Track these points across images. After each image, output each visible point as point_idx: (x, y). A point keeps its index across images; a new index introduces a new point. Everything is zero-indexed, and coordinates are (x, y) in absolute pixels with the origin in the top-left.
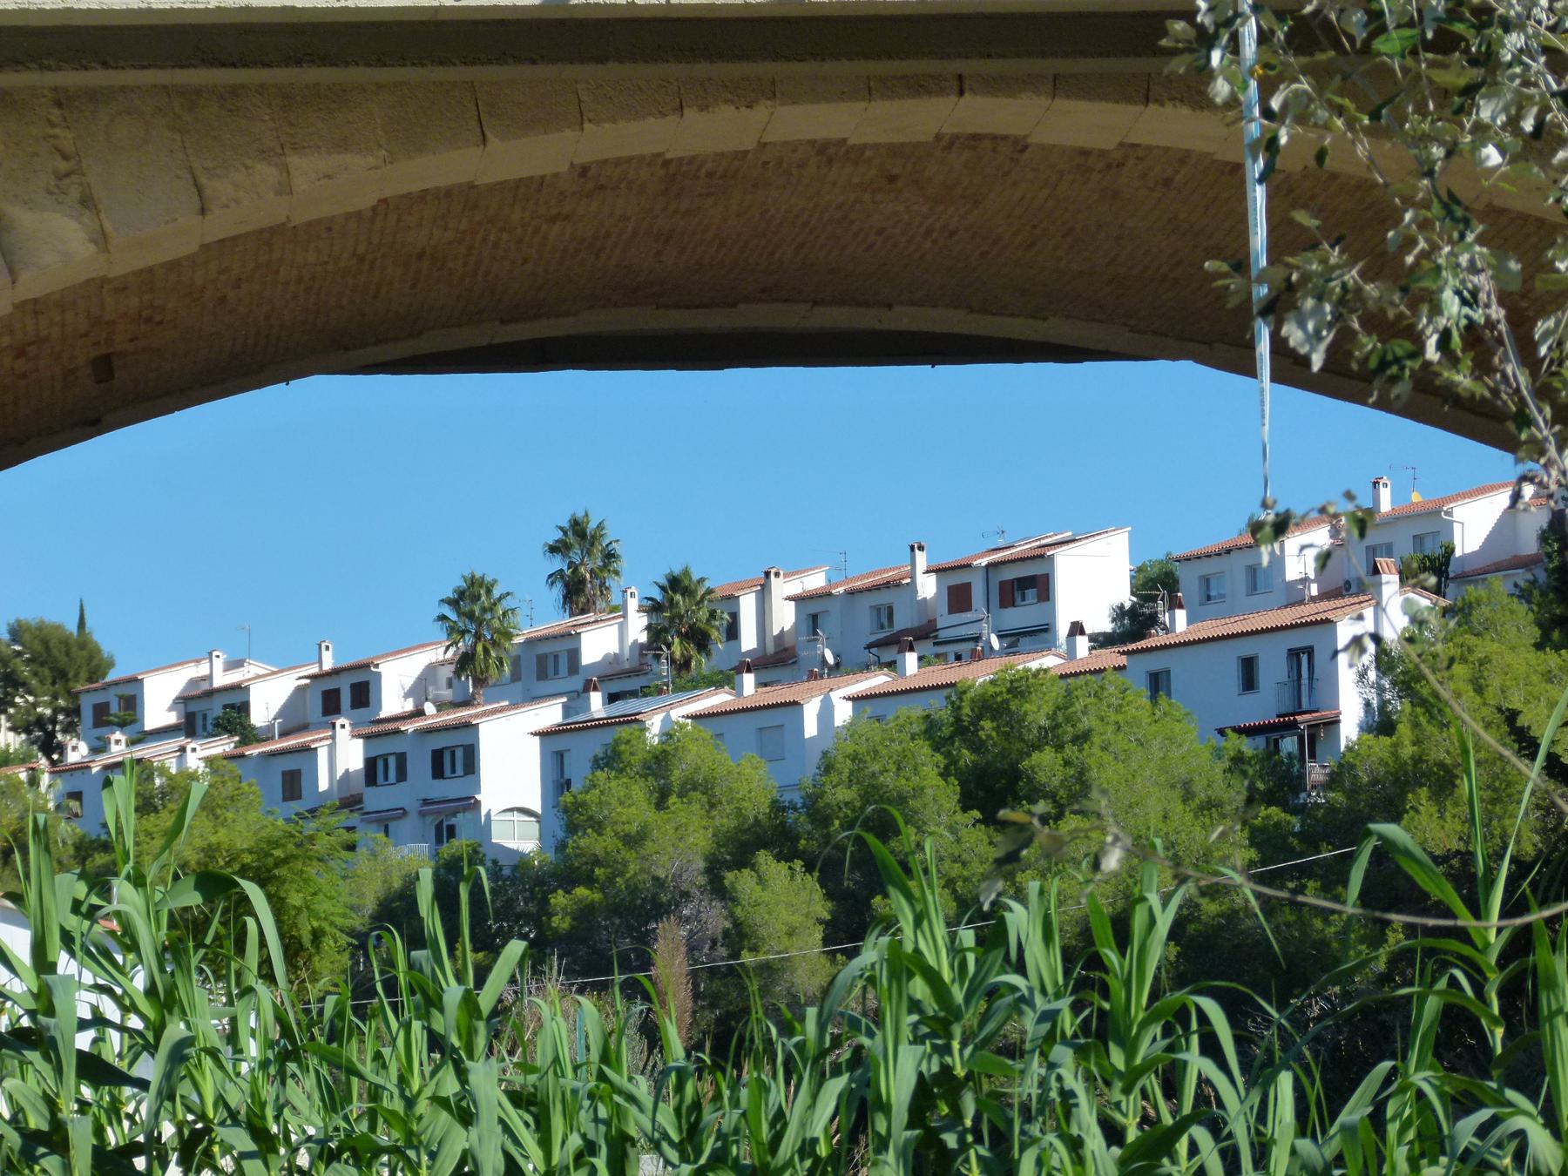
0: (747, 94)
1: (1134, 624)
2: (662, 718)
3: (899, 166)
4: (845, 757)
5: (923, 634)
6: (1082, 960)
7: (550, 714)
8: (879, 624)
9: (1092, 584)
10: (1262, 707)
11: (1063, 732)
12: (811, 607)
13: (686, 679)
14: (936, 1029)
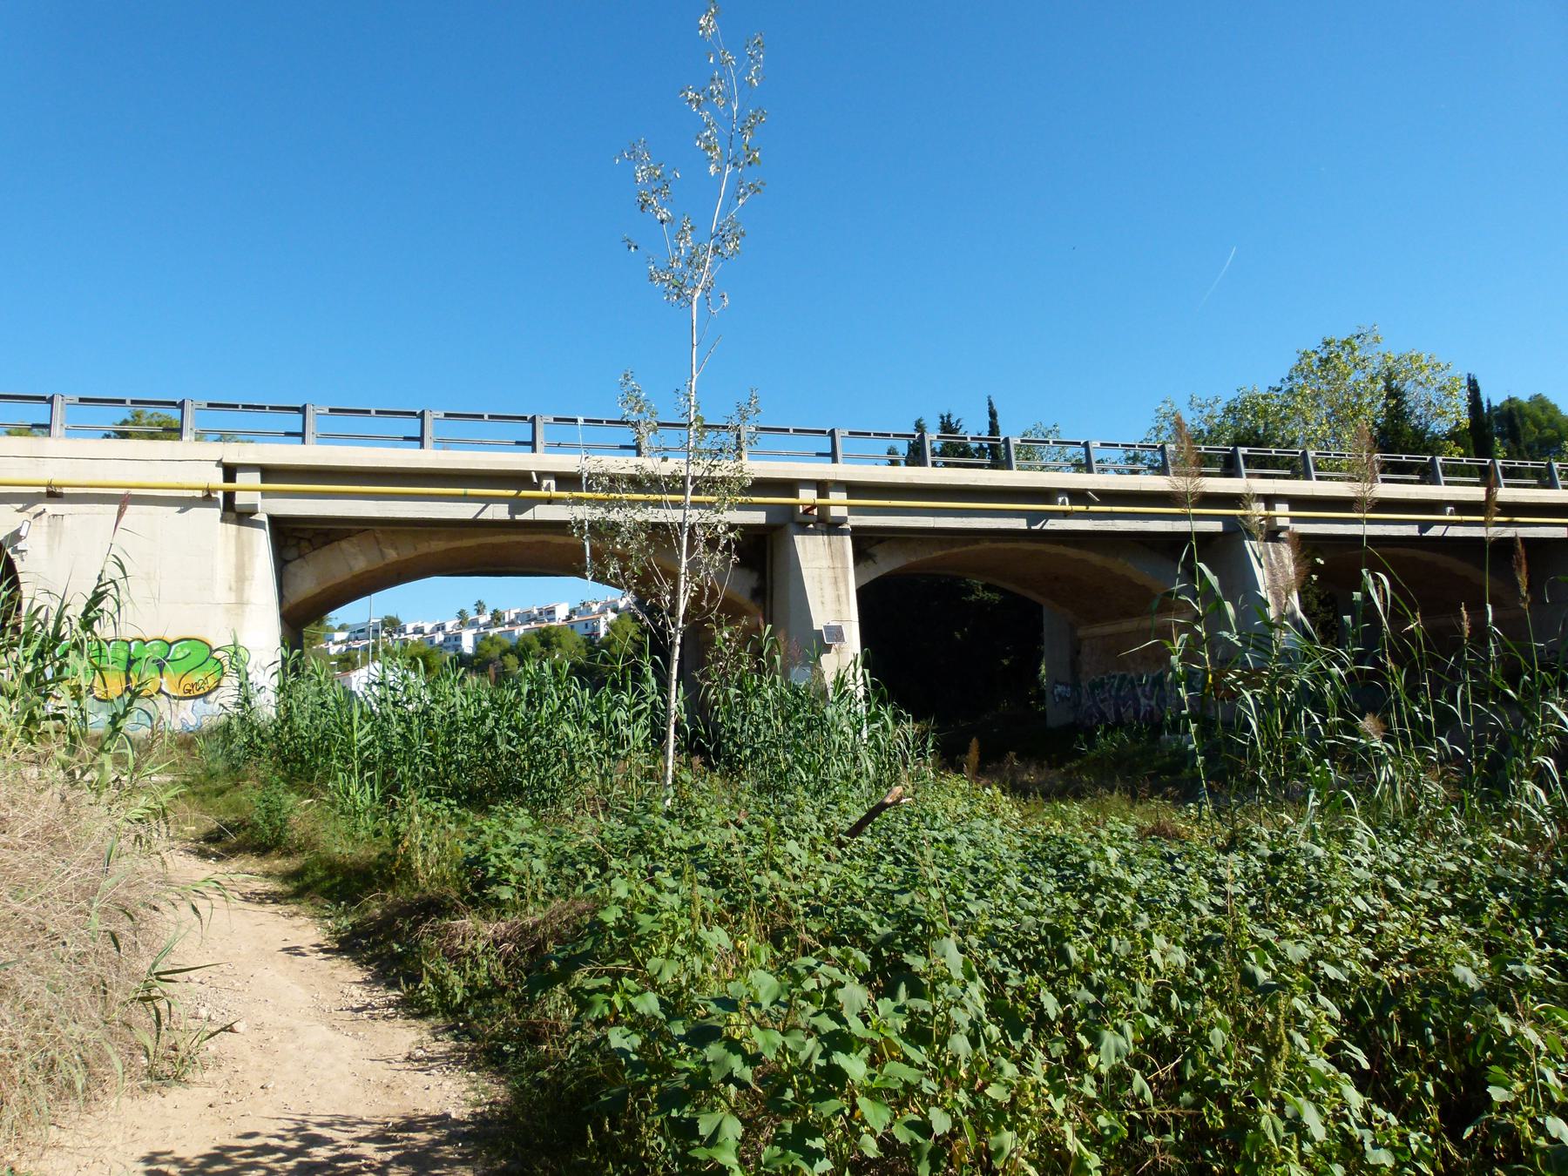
0: (506, 533)
1: (569, 618)
2: (492, 632)
3: (529, 546)
4: (522, 639)
5: (535, 619)
6: (555, 673)
7: (475, 631)
8: (528, 618)
9: (562, 612)
10: (588, 631)
11: (557, 635)
12: (517, 615)
13: (496, 625)
14: (531, 682)
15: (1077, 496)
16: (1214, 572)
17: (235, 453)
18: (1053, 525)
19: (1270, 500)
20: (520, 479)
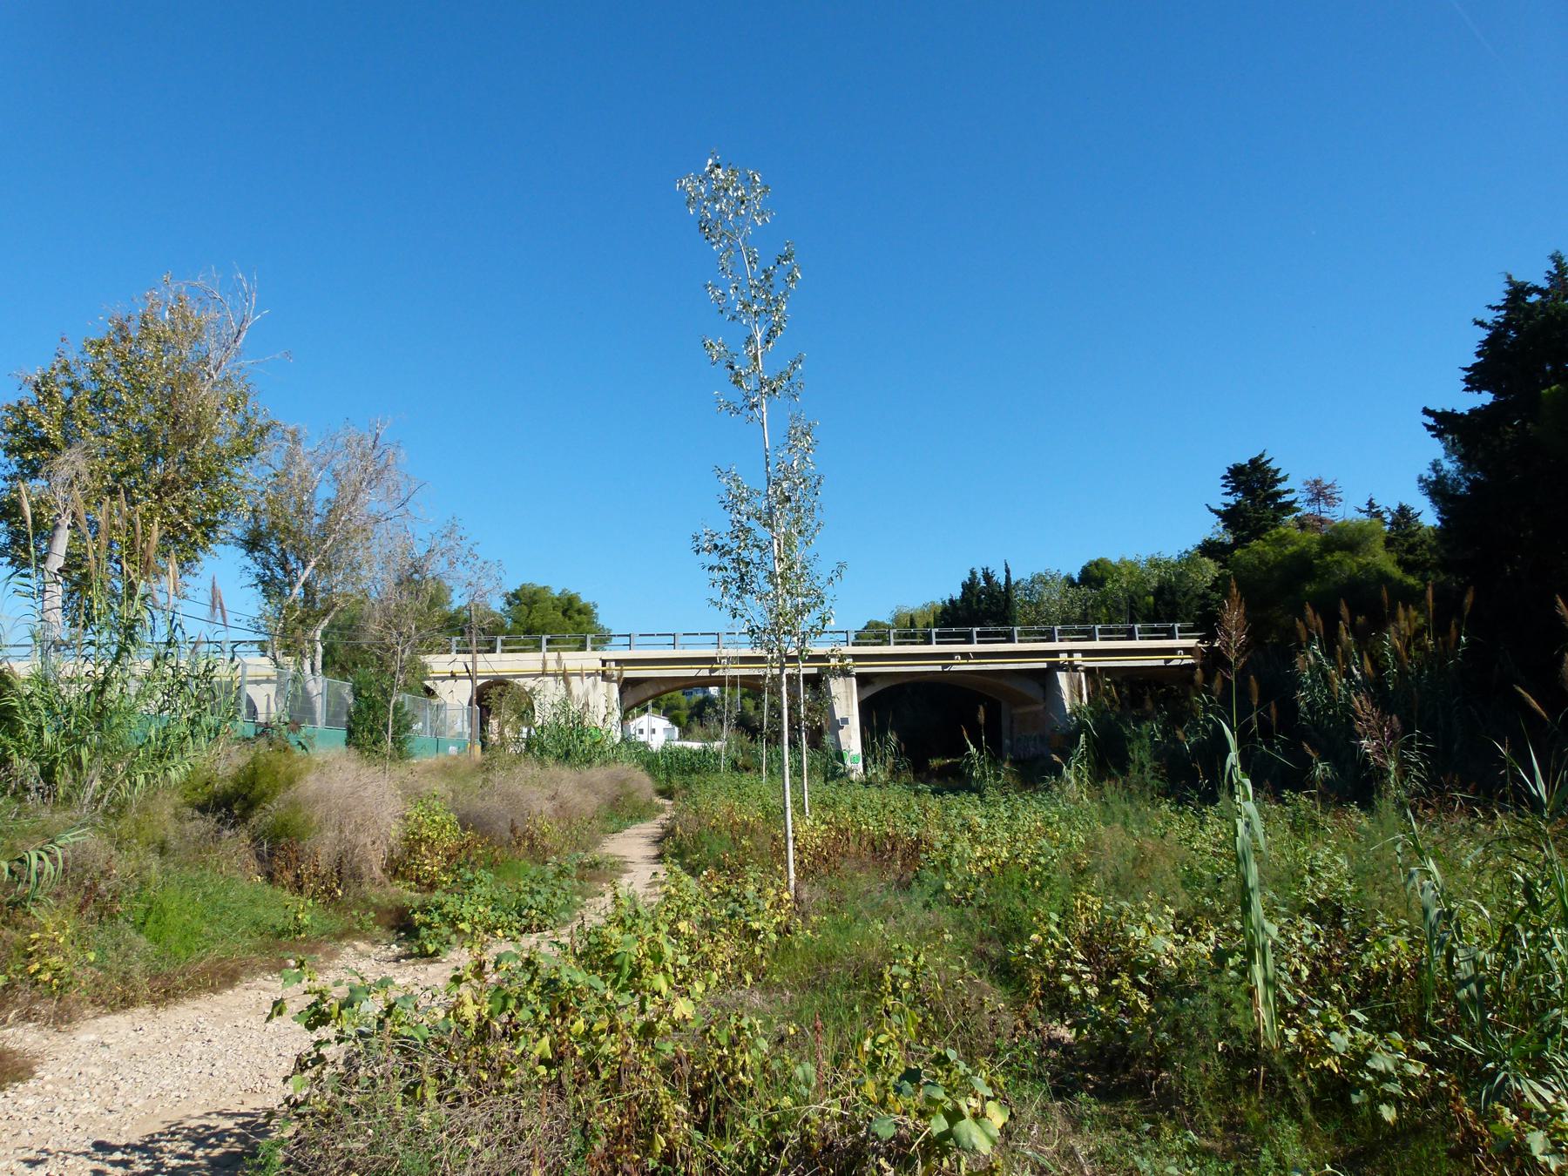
15: (965, 655)
16: (1534, 711)
17: (606, 655)
18: (954, 668)
19: (1070, 653)
20: (712, 660)
